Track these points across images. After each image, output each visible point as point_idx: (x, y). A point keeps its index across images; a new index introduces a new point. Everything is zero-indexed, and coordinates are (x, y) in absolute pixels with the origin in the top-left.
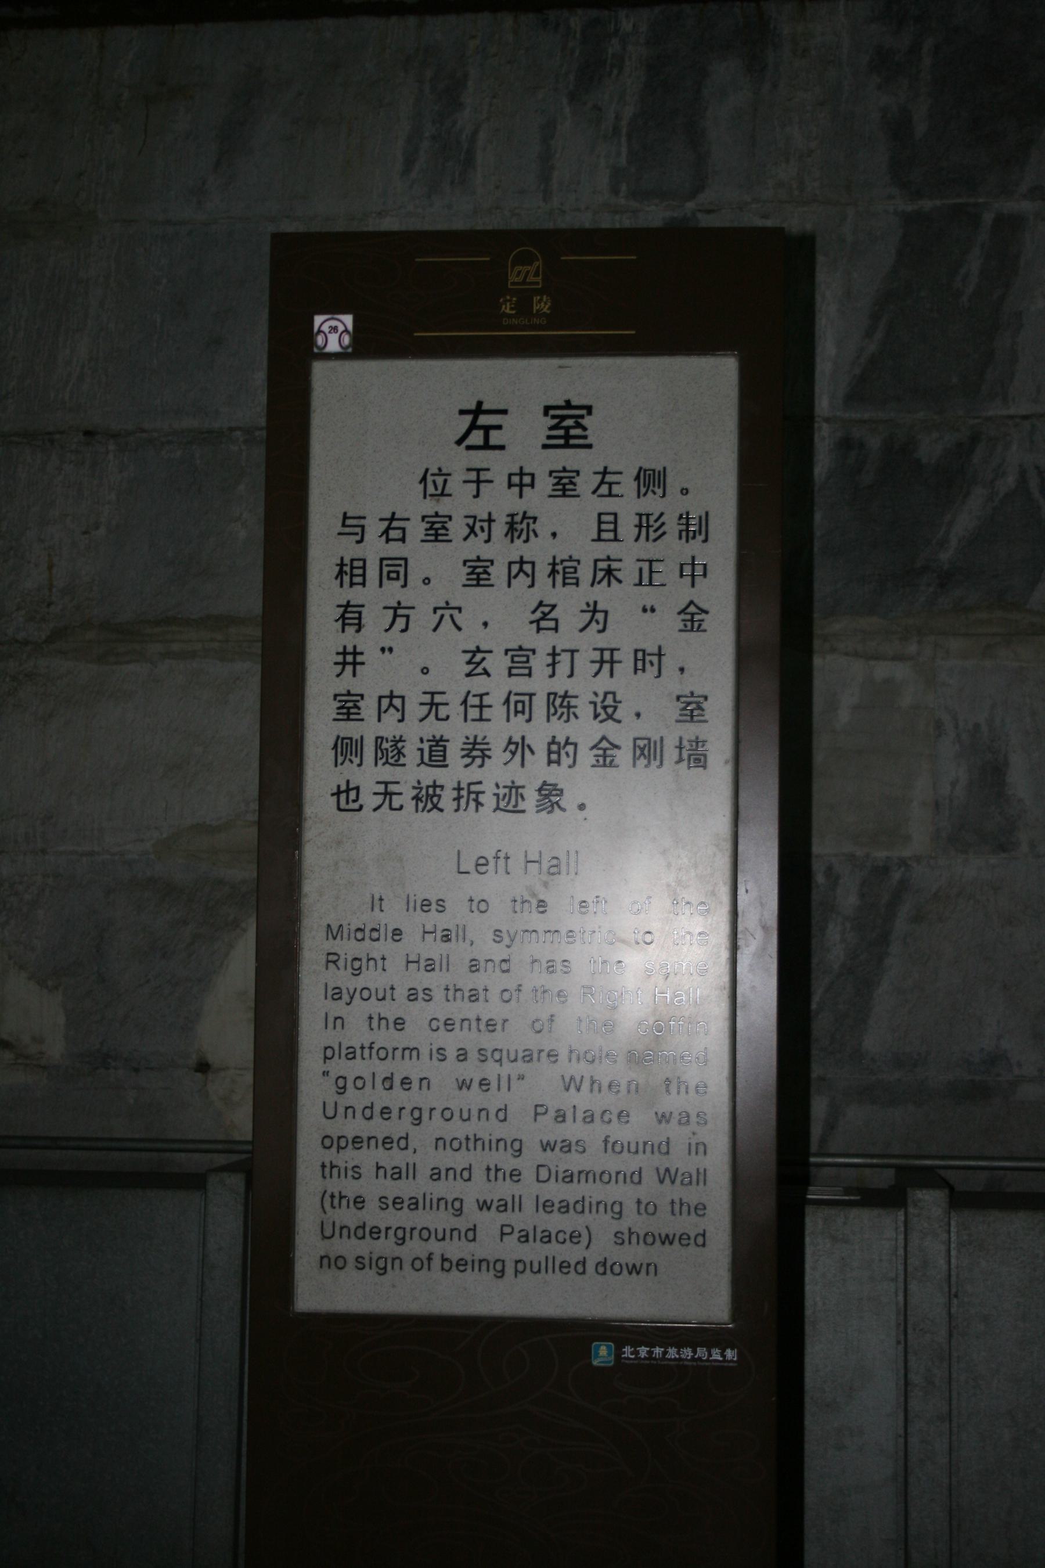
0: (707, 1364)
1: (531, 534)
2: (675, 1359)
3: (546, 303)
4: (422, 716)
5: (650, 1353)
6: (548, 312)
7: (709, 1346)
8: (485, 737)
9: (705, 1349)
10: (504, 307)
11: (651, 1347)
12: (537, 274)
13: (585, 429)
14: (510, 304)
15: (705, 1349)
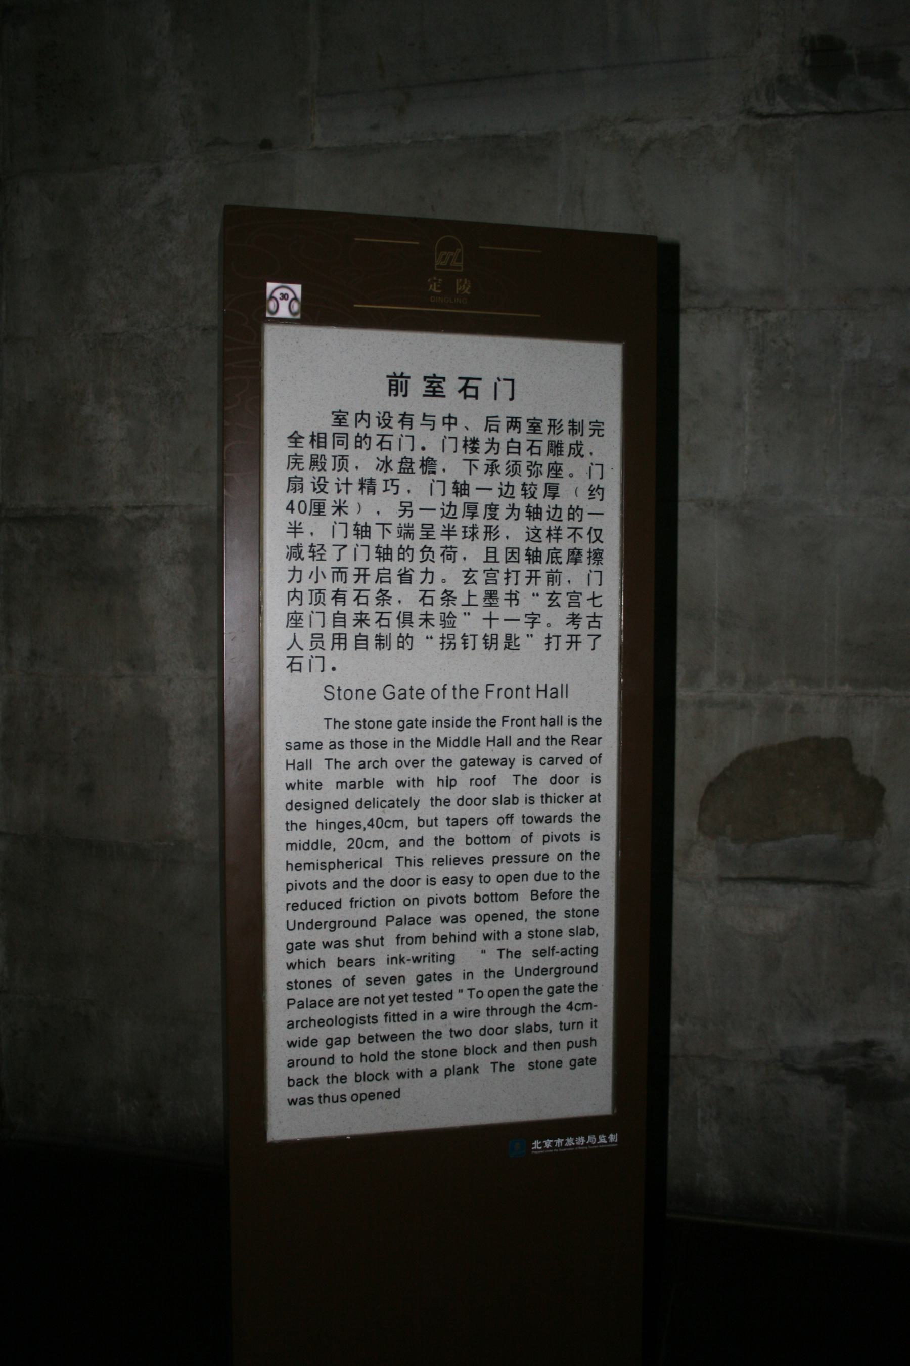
0: (595, 1147)
1: (539, 473)
2: (572, 1146)
3: (466, 286)
4: (290, 579)
5: (553, 1144)
6: (469, 293)
9: (594, 1136)
10: (431, 286)
11: (554, 1139)
12: (459, 260)
13: (442, 388)
14: (437, 284)
15: (594, 1136)
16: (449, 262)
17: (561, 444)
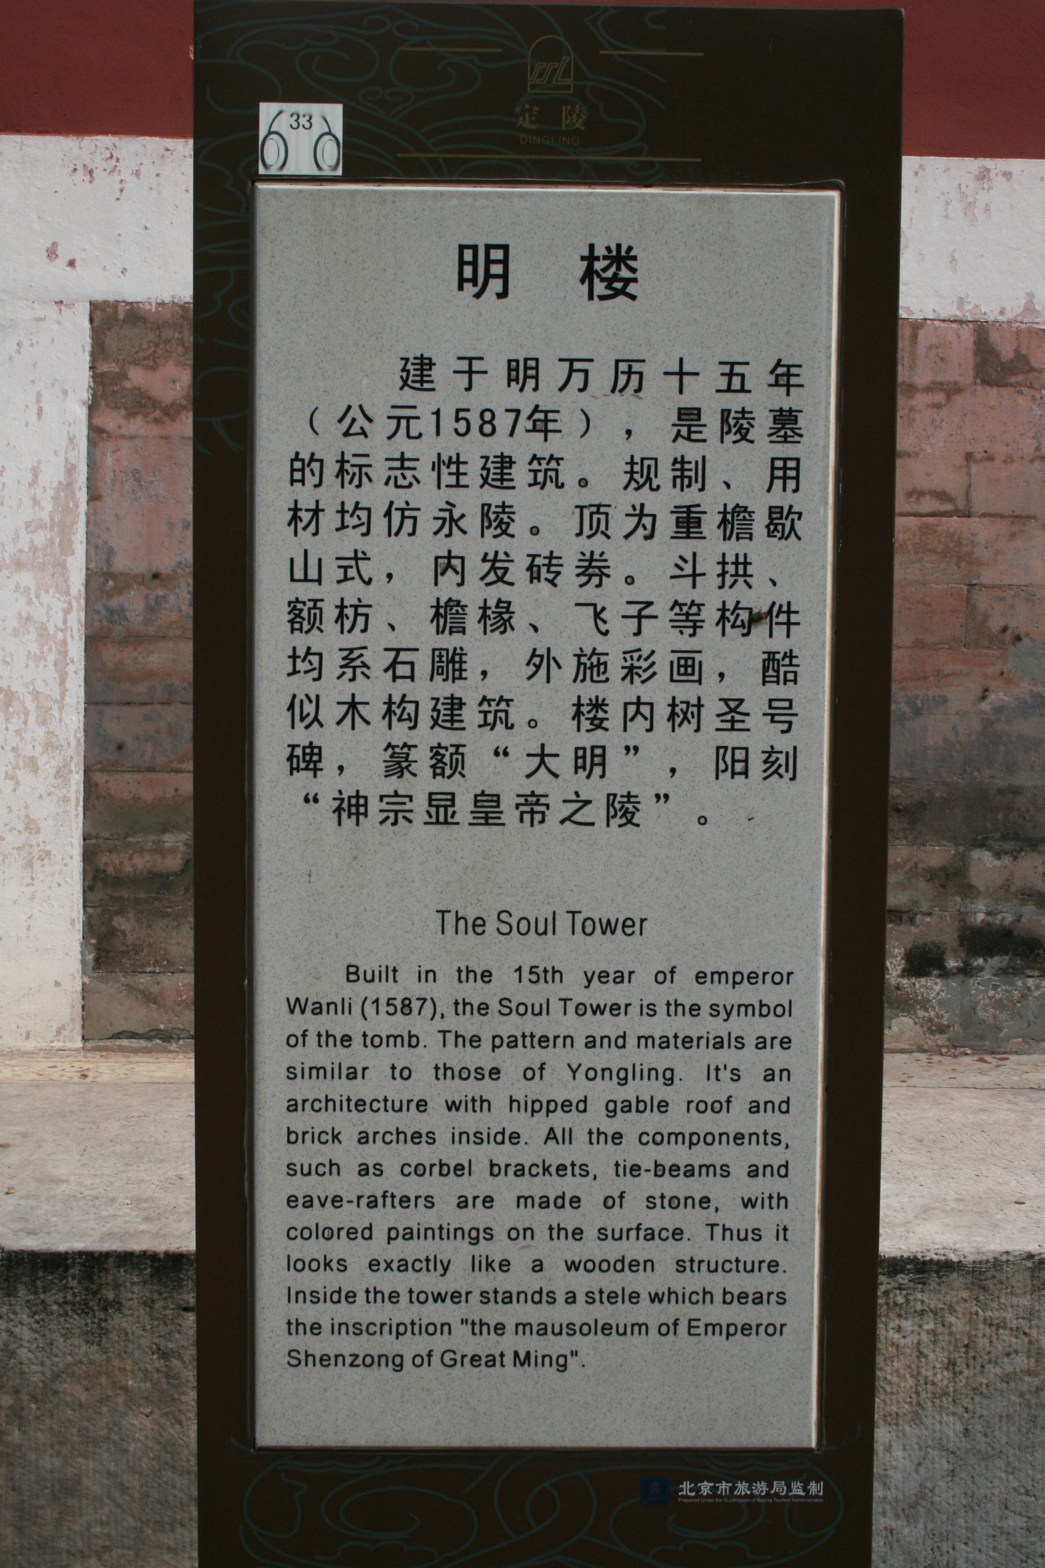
3: (579, 116)
5: (714, 1489)
6: (583, 128)
7: (788, 1478)
8: (602, 554)
12: (566, 75)
14: (530, 116)
16: (550, 81)
17: (461, 655)
